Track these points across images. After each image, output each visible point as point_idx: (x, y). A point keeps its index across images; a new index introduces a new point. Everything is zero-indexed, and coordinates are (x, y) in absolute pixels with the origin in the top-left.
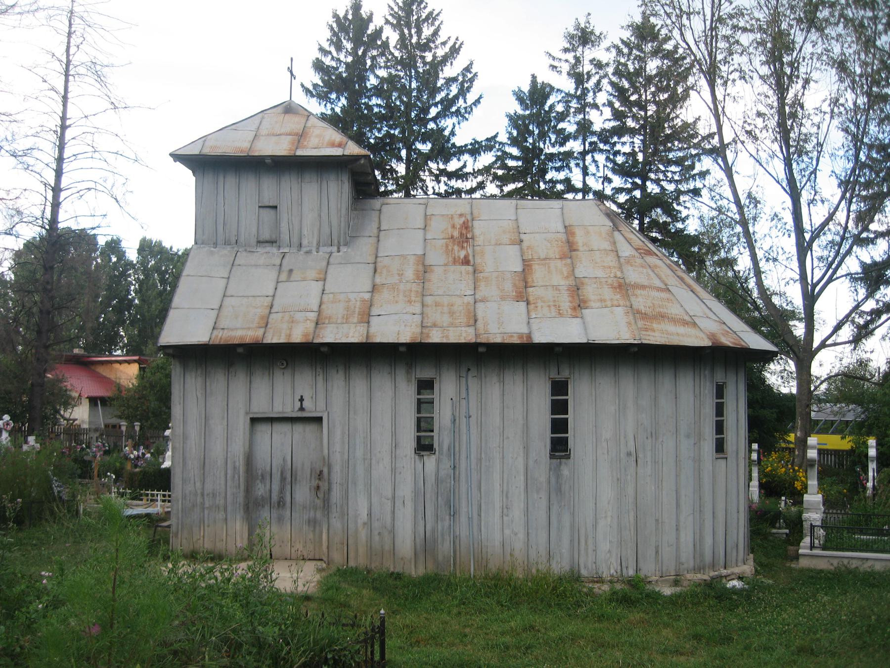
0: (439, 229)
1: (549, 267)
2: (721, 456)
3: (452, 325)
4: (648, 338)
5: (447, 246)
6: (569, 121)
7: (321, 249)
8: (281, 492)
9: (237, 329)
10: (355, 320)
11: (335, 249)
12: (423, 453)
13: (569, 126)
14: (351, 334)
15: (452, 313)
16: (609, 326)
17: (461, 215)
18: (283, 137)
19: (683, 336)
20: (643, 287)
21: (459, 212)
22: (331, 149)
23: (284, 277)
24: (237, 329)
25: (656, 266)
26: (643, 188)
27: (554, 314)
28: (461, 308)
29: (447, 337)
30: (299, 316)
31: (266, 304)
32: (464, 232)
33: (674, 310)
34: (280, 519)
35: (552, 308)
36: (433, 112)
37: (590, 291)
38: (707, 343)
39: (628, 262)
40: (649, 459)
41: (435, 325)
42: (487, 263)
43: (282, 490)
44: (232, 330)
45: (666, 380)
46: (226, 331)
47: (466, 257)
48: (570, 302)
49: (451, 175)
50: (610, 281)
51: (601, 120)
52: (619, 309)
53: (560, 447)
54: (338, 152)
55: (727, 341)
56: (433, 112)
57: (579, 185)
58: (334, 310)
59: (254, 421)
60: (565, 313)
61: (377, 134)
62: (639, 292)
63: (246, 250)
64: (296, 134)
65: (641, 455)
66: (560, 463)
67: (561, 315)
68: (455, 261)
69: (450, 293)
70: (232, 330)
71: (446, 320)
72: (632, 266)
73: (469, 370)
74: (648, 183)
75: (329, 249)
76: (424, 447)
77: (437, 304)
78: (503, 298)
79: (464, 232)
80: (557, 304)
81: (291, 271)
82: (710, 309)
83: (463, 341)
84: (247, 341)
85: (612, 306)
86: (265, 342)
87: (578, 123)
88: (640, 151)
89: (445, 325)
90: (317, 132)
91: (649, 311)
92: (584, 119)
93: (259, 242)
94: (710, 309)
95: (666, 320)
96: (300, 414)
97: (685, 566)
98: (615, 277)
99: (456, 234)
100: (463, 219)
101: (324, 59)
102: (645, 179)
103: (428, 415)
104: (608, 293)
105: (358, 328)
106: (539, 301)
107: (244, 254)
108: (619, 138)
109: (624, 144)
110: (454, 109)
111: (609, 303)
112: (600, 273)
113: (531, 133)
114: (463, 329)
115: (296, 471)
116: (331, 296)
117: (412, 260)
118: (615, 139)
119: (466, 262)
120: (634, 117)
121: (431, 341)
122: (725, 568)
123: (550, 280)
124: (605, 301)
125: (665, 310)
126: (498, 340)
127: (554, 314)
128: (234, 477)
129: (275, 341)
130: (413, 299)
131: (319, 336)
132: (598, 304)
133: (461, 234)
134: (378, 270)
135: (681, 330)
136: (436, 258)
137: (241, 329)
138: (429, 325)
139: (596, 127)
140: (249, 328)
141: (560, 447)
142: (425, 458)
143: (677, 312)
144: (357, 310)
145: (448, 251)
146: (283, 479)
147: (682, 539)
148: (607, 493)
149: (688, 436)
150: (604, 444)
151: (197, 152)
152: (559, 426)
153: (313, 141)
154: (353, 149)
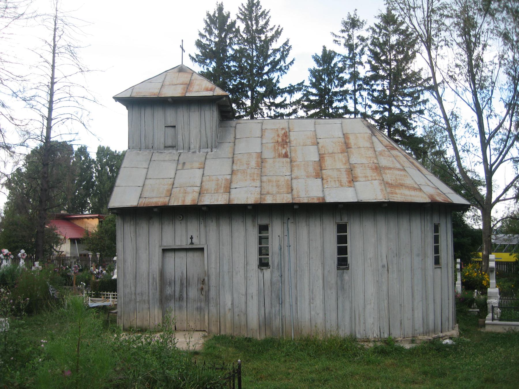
0: (270, 137)
1: (334, 158)
6: (345, 73)
9: (153, 198)
10: (222, 191)
11: (209, 150)
12: (263, 268)
13: (346, 76)
14: (220, 200)
15: (278, 186)
16: (370, 192)
17: (283, 129)
18: (178, 86)
19: (414, 196)
20: (390, 168)
21: (281, 127)
22: (206, 92)
23: (180, 167)
24: (153, 198)
25: (397, 156)
26: (390, 110)
27: (338, 185)
29: (276, 200)
31: (170, 183)
32: (284, 138)
33: (408, 182)
34: (181, 308)
35: (337, 182)
36: (266, 69)
37: (358, 172)
40: (395, 269)
41: (268, 193)
43: (181, 291)
45: (404, 223)
46: (147, 199)
48: (347, 178)
49: (277, 106)
50: (370, 165)
53: (343, 263)
54: (210, 94)
55: (440, 199)
56: (266, 69)
57: (352, 110)
58: (209, 185)
59: (164, 251)
61: (234, 83)
62: (387, 171)
64: (186, 84)
65: (390, 267)
66: (343, 272)
67: (342, 186)
70: (151, 198)
71: (274, 190)
72: (383, 156)
73: (289, 219)
74: (393, 108)
75: (206, 150)
76: (263, 264)
77: (269, 181)
79: (284, 138)
80: (339, 179)
81: (184, 163)
82: (430, 181)
83: (285, 202)
84: (160, 204)
85: (372, 180)
86: (170, 205)
90: (198, 82)
91: (393, 182)
92: (354, 71)
93: (165, 147)
94: (430, 181)
95: (404, 188)
97: (418, 331)
98: (373, 163)
99: (280, 140)
100: (284, 131)
101: (202, 40)
102: (391, 105)
106: (329, 178)
107: (157, 154)
108: (375, 82)
109: (378, 85)
110: (278, 67)
111: (370, 178)
112: (364, 161)
113: (324, 80)
114: (285, 195)
116: (208, 177)
117: (254, 155)
118: (373, 82)
119: (286, 156)
122: (442, 332)
123: (335, 165)
124: (367, 177)
125: (403, 182)
126: (306, 201)
127: (338, 185)
129: (175, 204)
130: (255, 178)
132: (364, 179)
133: (283, 140)
134: (235, 162)
135: (413, 193)
136: (268, 154)
137: (156, 198)
138: (265, 193)
139: (362, 76)
140: (160, 197)
141: (343, 263)
142: (264, 270)
144: (223, 185)
146: (182, 284)
147: (416, 315)
148: (371, 290)
149: (418, 255)
150: (369, 261)
151: (129, 96)
152: (342, 251)
153: (196, 88)
154: (219, 92)
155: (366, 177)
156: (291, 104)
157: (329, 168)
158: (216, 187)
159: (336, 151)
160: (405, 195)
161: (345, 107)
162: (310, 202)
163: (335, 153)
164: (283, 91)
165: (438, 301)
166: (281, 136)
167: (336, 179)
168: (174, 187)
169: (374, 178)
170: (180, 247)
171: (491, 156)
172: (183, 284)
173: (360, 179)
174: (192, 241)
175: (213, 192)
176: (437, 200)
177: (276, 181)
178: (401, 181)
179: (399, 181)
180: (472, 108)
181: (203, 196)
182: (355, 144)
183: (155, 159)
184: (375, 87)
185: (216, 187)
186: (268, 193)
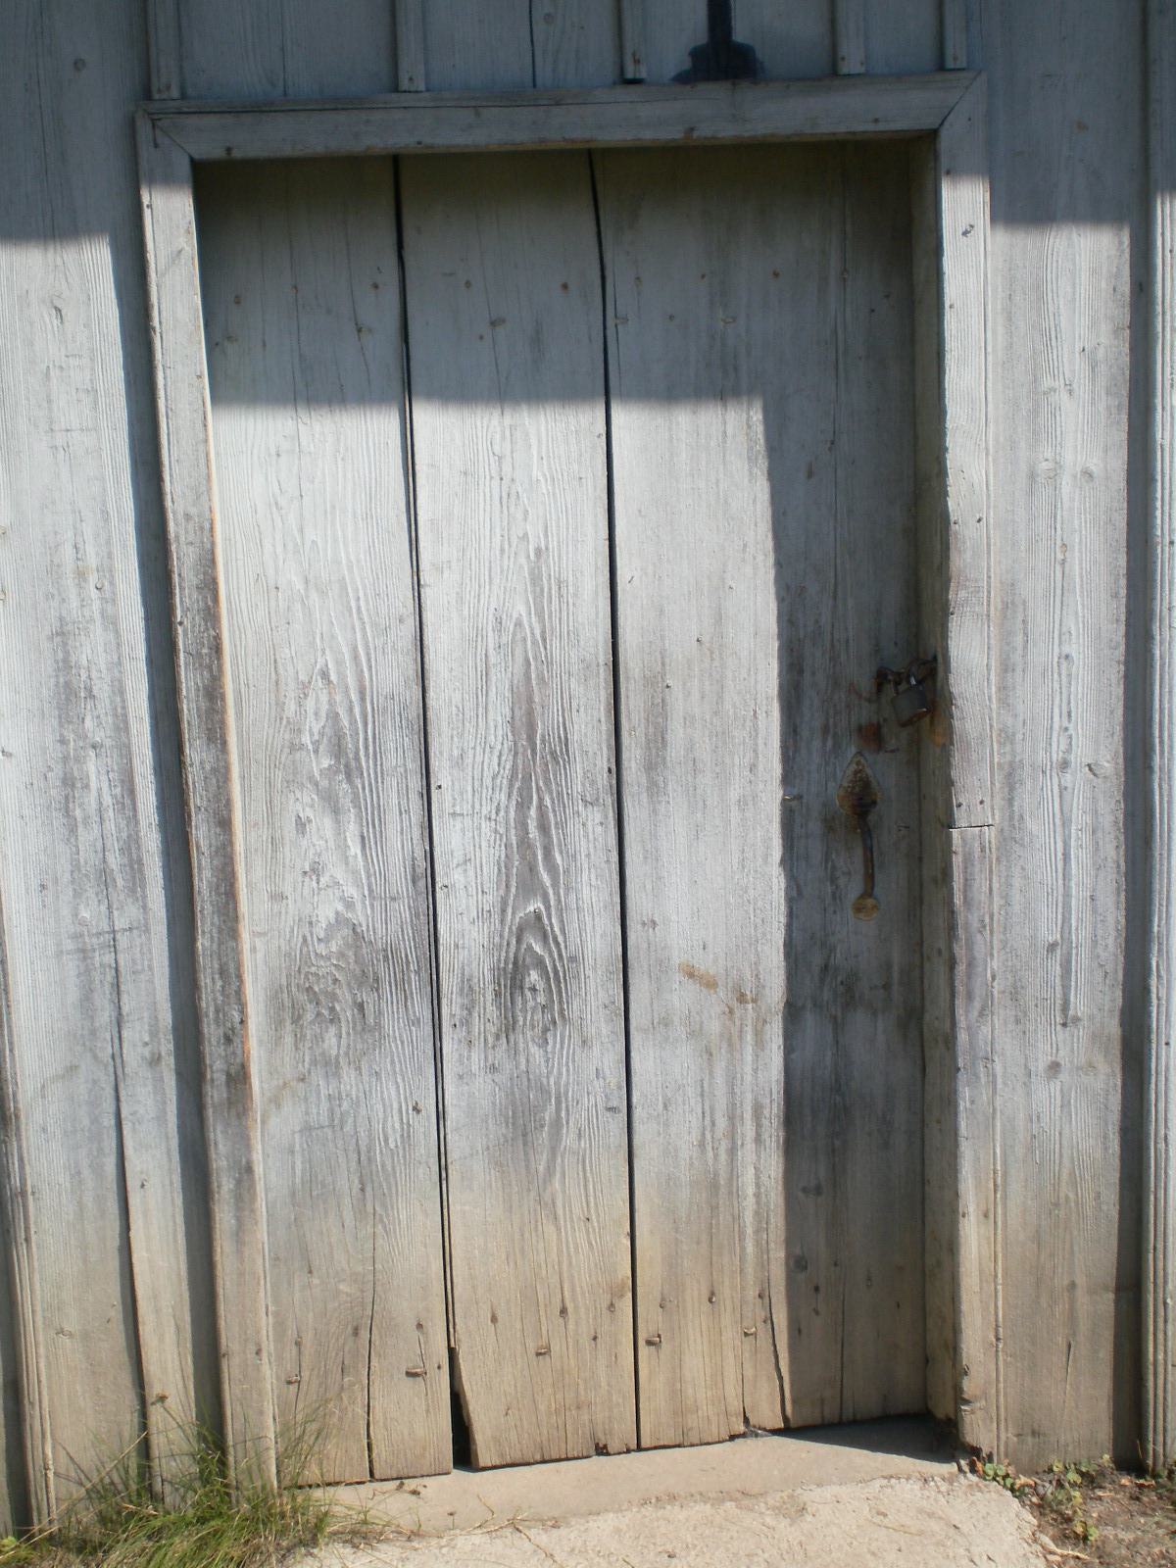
8: (529, 885)
43: (529, 865)
115: (658, 684)
146: (535, 755)
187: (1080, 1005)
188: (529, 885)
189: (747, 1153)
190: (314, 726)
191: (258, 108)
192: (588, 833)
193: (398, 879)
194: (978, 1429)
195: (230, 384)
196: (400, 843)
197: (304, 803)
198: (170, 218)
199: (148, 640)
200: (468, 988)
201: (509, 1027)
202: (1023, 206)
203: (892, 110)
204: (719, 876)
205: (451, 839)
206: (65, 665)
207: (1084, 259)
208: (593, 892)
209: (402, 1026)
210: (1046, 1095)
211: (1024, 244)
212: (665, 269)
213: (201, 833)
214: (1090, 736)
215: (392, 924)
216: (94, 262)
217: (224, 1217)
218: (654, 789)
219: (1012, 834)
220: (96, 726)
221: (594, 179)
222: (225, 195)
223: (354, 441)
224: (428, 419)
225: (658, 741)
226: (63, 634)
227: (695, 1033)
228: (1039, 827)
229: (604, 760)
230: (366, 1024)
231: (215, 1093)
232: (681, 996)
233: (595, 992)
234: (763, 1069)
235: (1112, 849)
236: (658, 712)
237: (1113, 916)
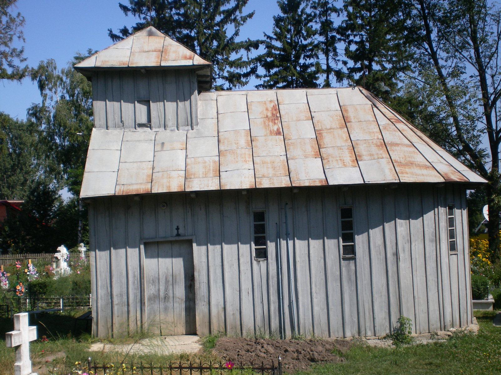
0: (258, 112)
1: (334, 134)
2: (453, 252)
3: (275, 175)
4: (404, 178)
5: (265, 123)
6: (316, 22)
7: (180, 128)
8: (166, 291)
9: (132, 184)
10: (211, 175)
11: (190, 127)
12: (259, 259)
13: (316, 26)
14: (210, 185)
15: (274, 168)
16: (378, 173)
17: (271, 101)
18: (151, 53)
19: (426, 176)
20: (397, 145)
21: (269, 100)
22: (185, 61)
23: (158, 148)
24: (132, 184)
25: (403, 130)
26: (369, 67)
27: (341, 165)
28: (279, 164)
29: (273, 183)
30: (174, 174)
31: (149, 167)
32: (274, 112)
33: (419, 159)
34: (166, 309)
35: (339, 161)
36: (218, 18)
37: (362, 149)
38: (441, 180)
39: (385, 128)
41: (264, 176)
42: (293, 134)
43: (166, 290)
44: (130, 185)
46: (125, 186)
47: (278, 130)
48: (350, 157)
49: (232, 64)
50: (374, 141)
51: (337, 20)
52: (383, 160)
54: (189, 63)
55: (455, 178)
56: (218, 18)
57: (324, 67)
58: (197, 169)
60: (348, 164)
61: (178, 35)
62: (395, 148)
63: (130, 131)
64: (159, 51)
67: (345, 166)
68: (271, 133)
69: (271, 154)
70: (130, 185)
71: (271, 172)
72: (388, 130)
73: (287, 204)
74: (374, 64)
75: (186, 128)
77: (264, 163)
78: (306, 157)
79: (274, 112)
80: (342, 158)
81: (163, 144)
82: (441, 157)
83: (284, 186)
84: (142, 192)
85: (378, 158)
86: (153, 192)
87: (322, 23)
88: (367, 41)
89: (270, 175)
90: (173, 49)
91: (402, 161)
92: (326, 20)
94: (441, 157)
95: (414, 166)
96: (177, 238)
98: (378, 139)
99: (270, 114)
100: (272, 104)
102: (371, 61)
103: (262, 235)
104: (374, 150)
105: (214, 180)
106: (330, 157)
107: (130, 133)
108: (352, 31)
109: (355, 36)
110: (233, 17)
111: (376, 157)
112: (367, 137)
113: (289, 31)
114: (283, 178)
115: (176, 276)
116: (193, 159)
117: (243, 133)
118: (349, 32)
119: (278, 133)
120: (362, 18)
121: (263, 187)
122: (453, 327)
123: (335, 141)
124: (373, 155)
125: (413, 160)
126: (307, 184)
127: (341, 165)
128: (134, 282)
129: (160, 191)
130: (247, 159)
131: (188, 187)
132: (369, 157)
133: (273, 114)
134: (222, 141)
135: (425, 172)
136: (258, 131)
137: (136, 185)
138: (260, 176)
139: (336, 25)
140: (141, 184)
142: (261, 262)
143: (421, 161)
144: (211, 168)
145: (266, 126)
146: (167, 281)
151: (93, 66)
153: (172, 56)
154: (198, 60)
155: (371, 155)
156: (248, 63)
157: (329, 145)
158: (204, 170)
159: (334, 126)
160: (416, 175)
161: (318, 65)
162: (312, 185)
163: (333, 129)
164: (241, 46)
165: (455, 291)
166: (270, 109)
167: (338, 158)
168: (155, 171)
169: (380, 156)
170: (164, 240)
171: (497, 122)
172: (168, 282)
173: (365, 157)
174: (178, 232)
175: (201, 176)
176: (452, 179)
177: (271, 163)
178: (411, 159)
179: (408, 159)
180: (476, 68)
181: (189, 181)
182: (355, 117)
183: (129, 139)
184: (351, 38)
185: (204, 170)
186: (264, 176)
187: (205, 300)
188: (166, 291)
189: (183, 312)
190: (151, 279)
191: (148, 239)
192: (171, 287)
193: (157, 290)
194: (198, 333)
195: (147, 257)
196: (157, 288)
197: (150, 285)
198: (142, 247)
199: (172, 66)
200: (162, 298)
201: (165, 302)
202: (199, 244)
203: (190, 238)
204: (180, 291)
205: (161, 287)
206: (134, 274)
207: (204, 248)
208: (171, 292)
209: (157, 301)
210: (203, 307)
211: (199, 247)
212: (176, 248)
213: (142, 286)
214: (205, 280)
215: (156, 294)
216: (137, 249)
217: (143, 313)
218: (176, 284)
219: (200, 288)
220: (136, 279)
221: (171, 242)
222: (146, 244)
223: (154, 261)
224: (160, 259)
225: (176, 281)
226: (134, 272)
227: (179, 302)
228: (202, 287)
229: (172, 282)
230: (155, 301)
231: (143, 304)
232: (178, 300)
233: (171, 299)
234: (183, 306)
235: (207, 289)
236: (176, 279)
237: (208, 294)
